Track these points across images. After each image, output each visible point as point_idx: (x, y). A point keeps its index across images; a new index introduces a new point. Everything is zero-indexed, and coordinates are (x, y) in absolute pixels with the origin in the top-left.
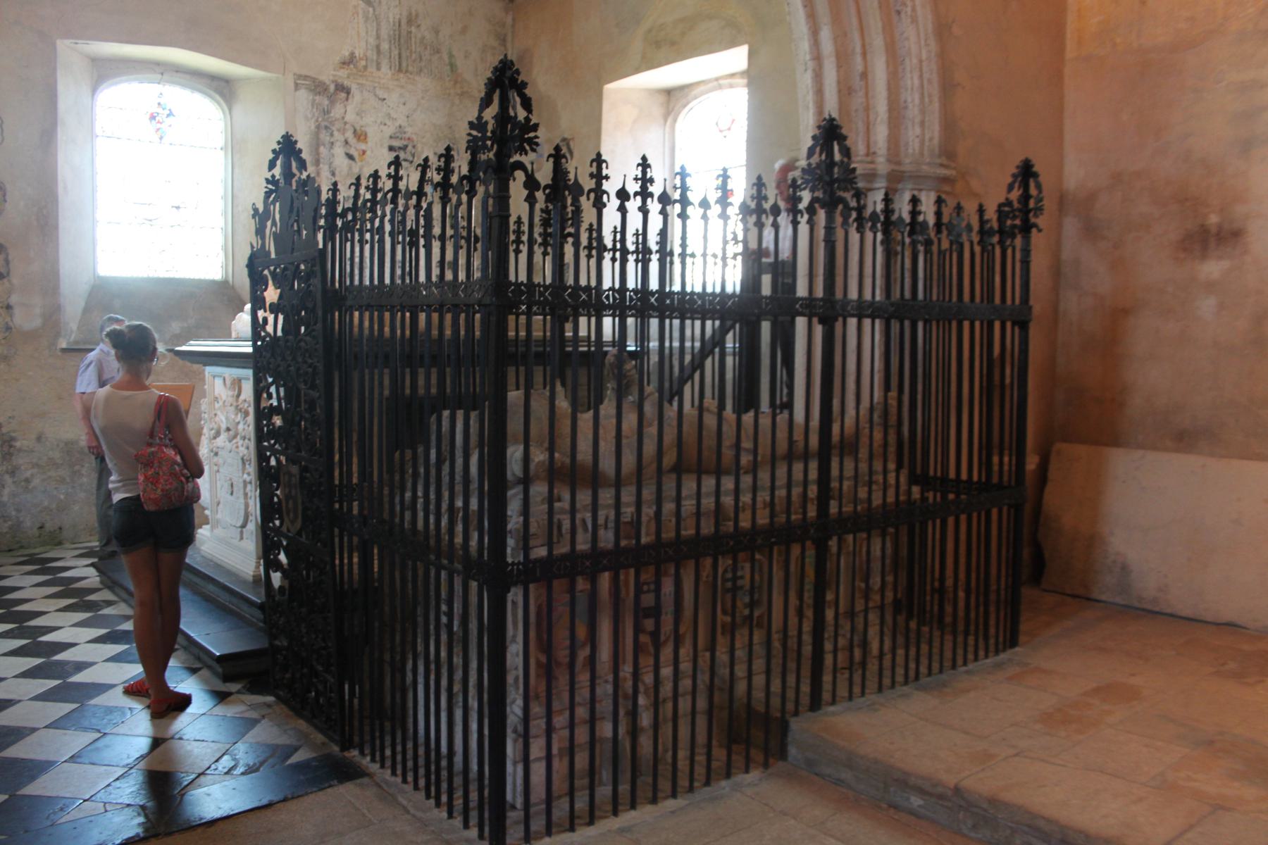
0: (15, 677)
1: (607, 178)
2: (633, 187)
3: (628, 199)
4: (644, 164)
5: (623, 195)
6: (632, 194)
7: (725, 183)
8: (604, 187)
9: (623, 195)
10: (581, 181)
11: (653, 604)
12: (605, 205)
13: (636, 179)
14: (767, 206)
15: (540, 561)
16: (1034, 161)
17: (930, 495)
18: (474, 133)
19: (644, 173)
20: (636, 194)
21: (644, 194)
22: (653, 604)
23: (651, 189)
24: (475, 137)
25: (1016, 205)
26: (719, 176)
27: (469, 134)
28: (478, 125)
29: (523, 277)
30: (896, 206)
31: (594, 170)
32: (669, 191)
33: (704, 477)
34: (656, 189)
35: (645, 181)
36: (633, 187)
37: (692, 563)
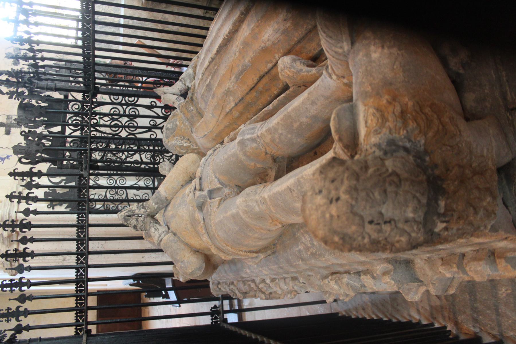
0: (187, 245)
2: (23, 206)
3: (21, 325)
6: (17, 323)
7: (11, 255)
10: (13, 327)
11: (95, 297)
13: (8, 321)
15: (99, 316)
18: (14, 97)
20: (17, 320)
21: (28, 199)
22: (95, 297)
25: (12, 89)
30: (11, 212)
31: (16, 200)
32: (24, 183)
33: (90, 249)
34: (14, 305)
35: (20, 197)
36: (23, 206)
37: (129, 119)
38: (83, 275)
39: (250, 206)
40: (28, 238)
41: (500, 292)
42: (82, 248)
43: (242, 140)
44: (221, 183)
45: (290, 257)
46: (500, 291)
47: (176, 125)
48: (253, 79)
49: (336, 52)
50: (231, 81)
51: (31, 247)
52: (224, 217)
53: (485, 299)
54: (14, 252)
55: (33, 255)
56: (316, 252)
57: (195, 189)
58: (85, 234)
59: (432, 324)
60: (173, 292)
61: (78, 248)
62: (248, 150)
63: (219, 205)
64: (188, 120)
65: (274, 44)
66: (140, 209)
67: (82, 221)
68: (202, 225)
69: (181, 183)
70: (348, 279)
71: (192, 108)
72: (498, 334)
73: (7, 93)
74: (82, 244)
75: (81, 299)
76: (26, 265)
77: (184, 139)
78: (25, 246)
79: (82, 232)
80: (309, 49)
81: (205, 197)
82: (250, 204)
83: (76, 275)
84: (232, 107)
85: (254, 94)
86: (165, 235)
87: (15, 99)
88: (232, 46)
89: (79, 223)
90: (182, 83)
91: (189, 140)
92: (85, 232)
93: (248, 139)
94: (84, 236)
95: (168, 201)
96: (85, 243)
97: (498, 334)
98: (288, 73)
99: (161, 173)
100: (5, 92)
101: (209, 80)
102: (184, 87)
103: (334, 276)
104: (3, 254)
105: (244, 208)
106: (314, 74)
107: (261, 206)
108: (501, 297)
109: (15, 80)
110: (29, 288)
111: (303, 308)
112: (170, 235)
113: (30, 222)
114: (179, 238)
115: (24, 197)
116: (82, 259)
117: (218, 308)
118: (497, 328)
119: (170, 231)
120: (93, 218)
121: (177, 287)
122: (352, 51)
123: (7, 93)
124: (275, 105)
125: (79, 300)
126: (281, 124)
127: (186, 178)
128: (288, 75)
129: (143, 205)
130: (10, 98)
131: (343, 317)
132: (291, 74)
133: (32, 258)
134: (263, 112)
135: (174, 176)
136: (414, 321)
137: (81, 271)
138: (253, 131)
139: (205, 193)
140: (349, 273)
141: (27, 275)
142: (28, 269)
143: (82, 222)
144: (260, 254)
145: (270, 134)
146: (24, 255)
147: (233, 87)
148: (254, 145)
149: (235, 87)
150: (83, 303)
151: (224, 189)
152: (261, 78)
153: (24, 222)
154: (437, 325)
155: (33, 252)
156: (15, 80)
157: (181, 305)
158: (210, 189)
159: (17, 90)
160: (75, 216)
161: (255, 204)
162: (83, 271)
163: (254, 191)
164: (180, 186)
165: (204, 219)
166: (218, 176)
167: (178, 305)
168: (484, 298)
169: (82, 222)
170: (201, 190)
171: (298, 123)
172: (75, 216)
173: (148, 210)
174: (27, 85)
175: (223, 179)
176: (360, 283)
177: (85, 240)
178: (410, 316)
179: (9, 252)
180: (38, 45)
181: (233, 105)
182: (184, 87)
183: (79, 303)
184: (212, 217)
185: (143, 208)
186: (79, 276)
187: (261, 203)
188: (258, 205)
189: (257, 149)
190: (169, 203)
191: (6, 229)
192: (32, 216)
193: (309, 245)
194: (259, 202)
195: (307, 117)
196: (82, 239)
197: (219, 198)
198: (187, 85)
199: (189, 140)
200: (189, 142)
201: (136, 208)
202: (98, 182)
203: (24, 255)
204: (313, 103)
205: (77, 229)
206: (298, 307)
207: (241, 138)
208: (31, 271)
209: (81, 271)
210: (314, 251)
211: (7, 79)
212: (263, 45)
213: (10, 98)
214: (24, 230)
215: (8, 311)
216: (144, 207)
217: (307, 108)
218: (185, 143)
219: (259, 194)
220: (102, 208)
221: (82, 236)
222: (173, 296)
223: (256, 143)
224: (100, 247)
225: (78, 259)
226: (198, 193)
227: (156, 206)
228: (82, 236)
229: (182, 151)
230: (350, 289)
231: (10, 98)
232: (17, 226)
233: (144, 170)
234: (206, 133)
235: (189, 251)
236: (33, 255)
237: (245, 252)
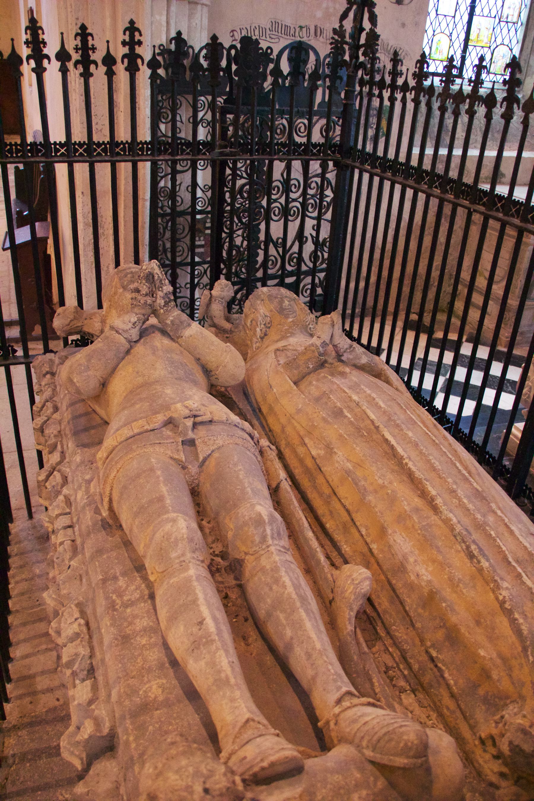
1: (140, 43)
4: (132, 28)
5: (109, 60)
7: (84, 42)
8: (137, 52)
9: (63, 56)
12: (45, 69)
14: (400, 82)
15: (500, 198)
16: (182, 32)
17: (239, 491)
18: (336, 37)
19: (132, 36)
23: (46, 51)
24: (337, 41)
26: (77, 35)
27: (333, 38)
28: (339, 32)
29: (77, 167)
36: (119, 52)
38: (56, 154)
39: (177, 545)
40: (114, 68)
41: (63, 792)
42: (99, 150)
43: (265, 522)
44: (205, 460)
45: (105, 556)
46: (66, 790)
48: (347, 498)
49: (363, 738)
50: (345, 461)
51: (99, 73)
52: (158, 477)
53: (52, 770)
54: (90, 46)
55: (86, 75)
56: (116, 610)
57: (195, 416)
58: (120, 154)
59: (9, 680)
60: (30, 238)
61: (99, 145)
62: (251, 530)
63: (175, 459)
64: (295, 359)
65: (390, 546)
66: (163, 298)
67: (142, 150)
68: (145, 428)
69: (202, 358)
70: (84, 655)
71: (311, 366)
72: (8, 792)
73: (341, 26)
74: (105, 150)
75: (18, 151)
76: (70, 65)
77: (266, 327)
78: (100, 63)
79: (124, 149)
80: (381, 596)
81: (186, 434)
82: (180, 545)
83: (55, 143)
84: (311, 450)
85: (327, 491)
86: (125, 338)
87: (333, 38)
88: (393, 471)
89: (138, 144)
90: (347, 349)
91: (266, 335)
92: (125, 154)
93: (265, 530)
94: (118, 154)
95: (175, 339)
96: (106, 155)
97: (8, 792)
98: (350, 591)
99: (216, 284)
100: (344, 23)
101: (349, 415)
102: (342, 350)
103: (84, 629)
104: (87, 29)
105: (174, 536)
106: (346, 629)
107: (177, 561)
108: (58, 794)
109: (362, 41)
110: (33, 70)
111: (16, 456)
112: (127, 345)
113: (138, 70)
114: (123, 358)
115: (135, 49)
116: (81, 151)
117: (13, 354)
118: (14, 789)
119: (132, 344)
120: (145, 169)
121: (37, 243)
122: (363, 759)
123: (341, 26)
124: (311, 543)
125: (16, 148)
126: (284, 592)
128: (346, 591)
129: (170, 301)
130: (334, 30)
131: (7, 532)
132: (347, 595)
133: (81, 75)
134: (301, 519)
135: (213, 348)
136: (11, 649)
137: (63, 151)
138: (275, 535)
139: (191, 435)
140: (91, 657)
141: (52, 69)
142: (63, 69)
143: (140, 149)
144: (107, 513)
145: (272, 570)
146: (86, 62)
147: (337, 462)
148: (257, 539)
149: (337, 465)
150: (12, 153)
151: (197, 464)
152: (348, 511)
153: (139, 61)
154: (8, 686)
155: (92, 75)
156: (362, 41)
157: (8, 253)
158: (197, 442)
159: (346, 43)
160: (149, 139)
161: (179, 552)
162: (63, 155)
163: (197, 546)
164: (198, 356)
165: (153, 430)
166: (216, 455)
167: (8, 245)
168: (55, 768)
169: (140, 149)
170: (195, 425)
171: (284, 622)
172: (149, 139)
173: (162, 311)
174: (354, 60)
175: (211, 463)
176: (78, 671)
177: (112, 156)
178: (18, 643)
179: (90, 38)
180: (413, 100)
181: (314, 453)
182: (342, 350)
183: (11, 148)
184: (157, 448)
185: (165, 302)
186: (55, 147)
187: (181, 562)
188: (179, 557)
189: (252, 542)
190: (172, 339)
191: (127, 33)
192: (149, 72)
193: (125, 598)
194: (182, 559)
195: (292, 638)
196: (114, 151)
197: (184, 459)
198: (345, 354)
199: (266, 335)
200: (263, 335)
201: (165, 291)
202: (200, 126)
203: (86, 62)
204: (309, 655)
205: (129, 141)
206: (16, 449)
207: (267, 521)
208: (60, 73)
209: (63, 151)
210: (117, 607)
211: (364, 30)
212: (390, 531)
213: (335, 31)
214: (126, 61)
215: (91, 49)
216: (166, 303)
217: (303, 643)
218: (261, 330)
219: (194, 558)
220: (159, 134)
221: (117, 150)
222: (23, 235)
223: (260, 542)
224: (97, 126)
225: (81, 145)
226: (189, 423)
227: (168, 322)
228: (117, 150)
229: (249, 321)
230: (71, 658)
231: (334, 30)
232: (132, 49)
233: (222, 200)
234: (275, 390)
235: (104, 376)
236: (86, 75)
237: (111, 494)
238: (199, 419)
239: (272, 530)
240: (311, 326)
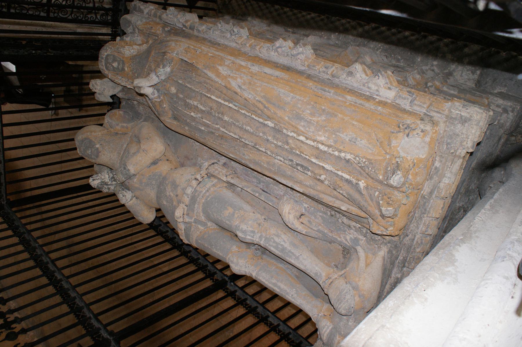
47: (123, 69)
127: (152, 161)
138: (252, 234)
238: (185, 212)
239: (249, 235)
240: (132, 51)
